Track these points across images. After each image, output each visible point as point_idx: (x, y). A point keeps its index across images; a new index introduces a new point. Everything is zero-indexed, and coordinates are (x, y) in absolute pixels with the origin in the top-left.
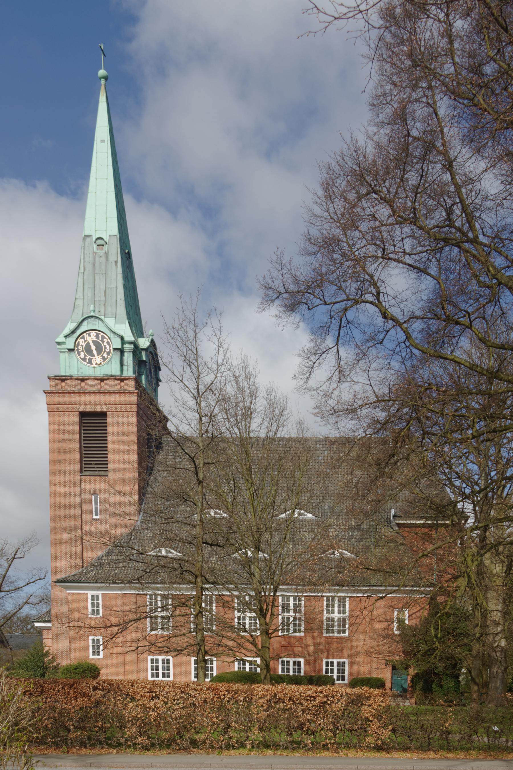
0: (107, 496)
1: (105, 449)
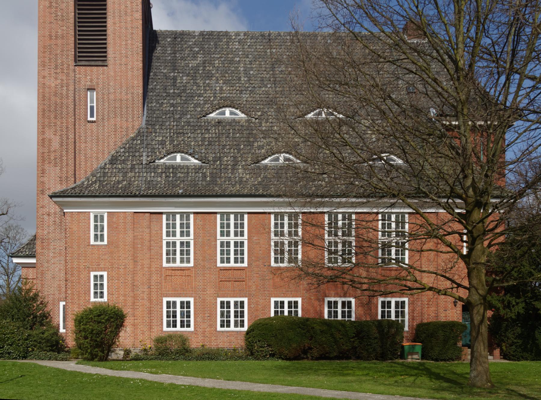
0: (106, 92)
1: (103, 33)
